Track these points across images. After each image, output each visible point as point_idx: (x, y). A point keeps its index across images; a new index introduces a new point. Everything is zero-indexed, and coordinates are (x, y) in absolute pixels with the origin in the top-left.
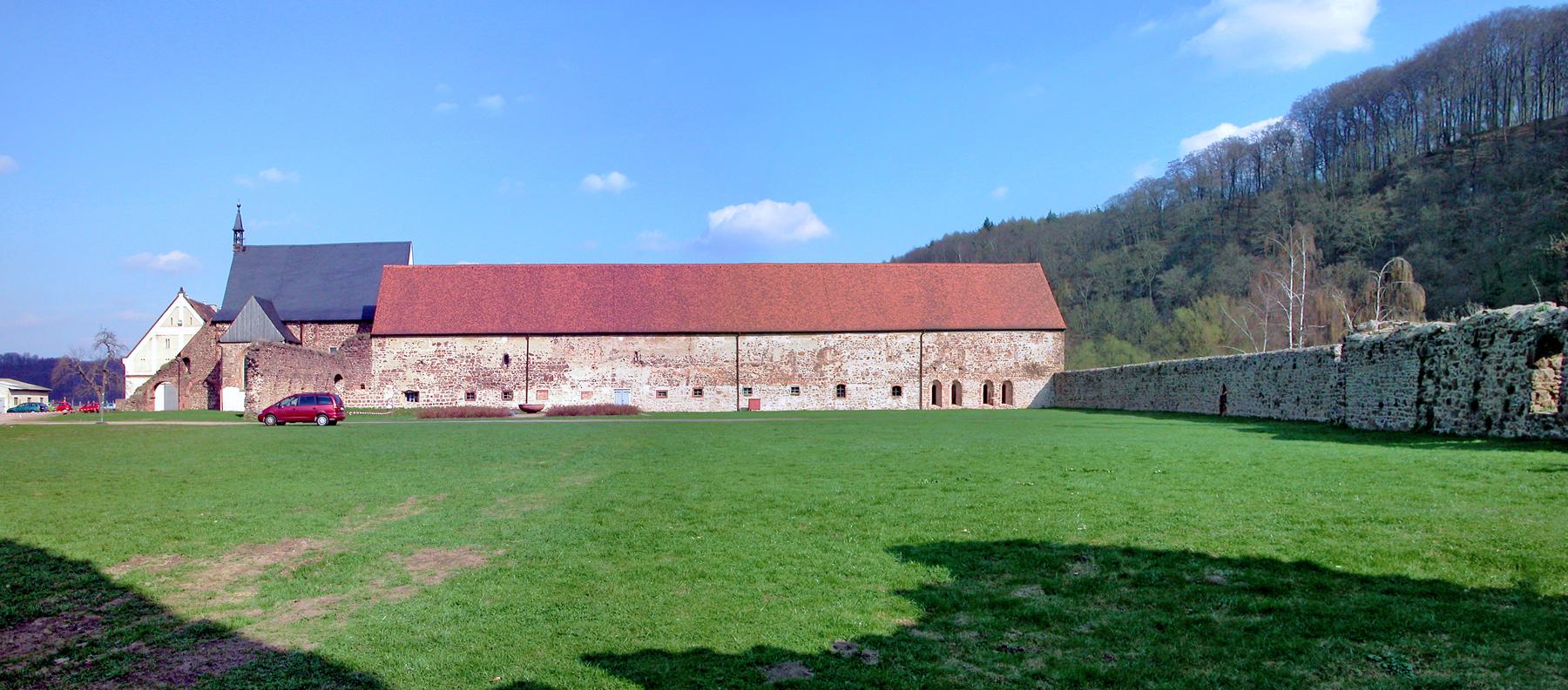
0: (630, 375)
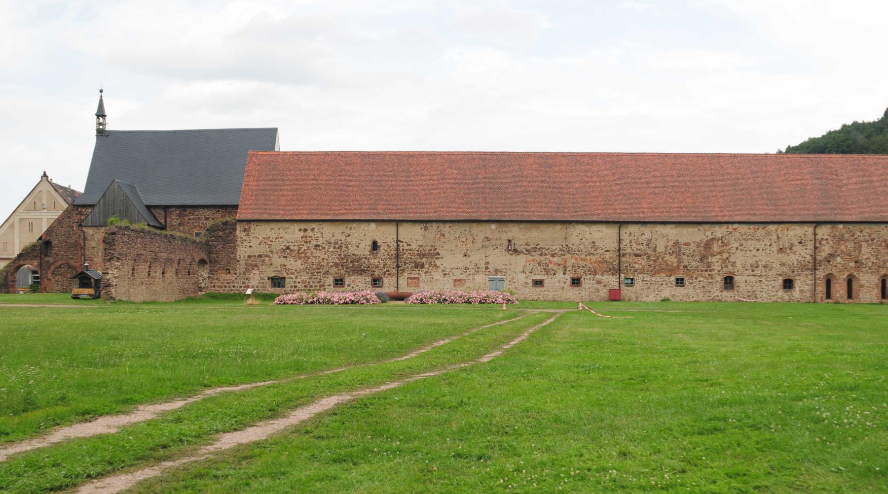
0: (504, 263)
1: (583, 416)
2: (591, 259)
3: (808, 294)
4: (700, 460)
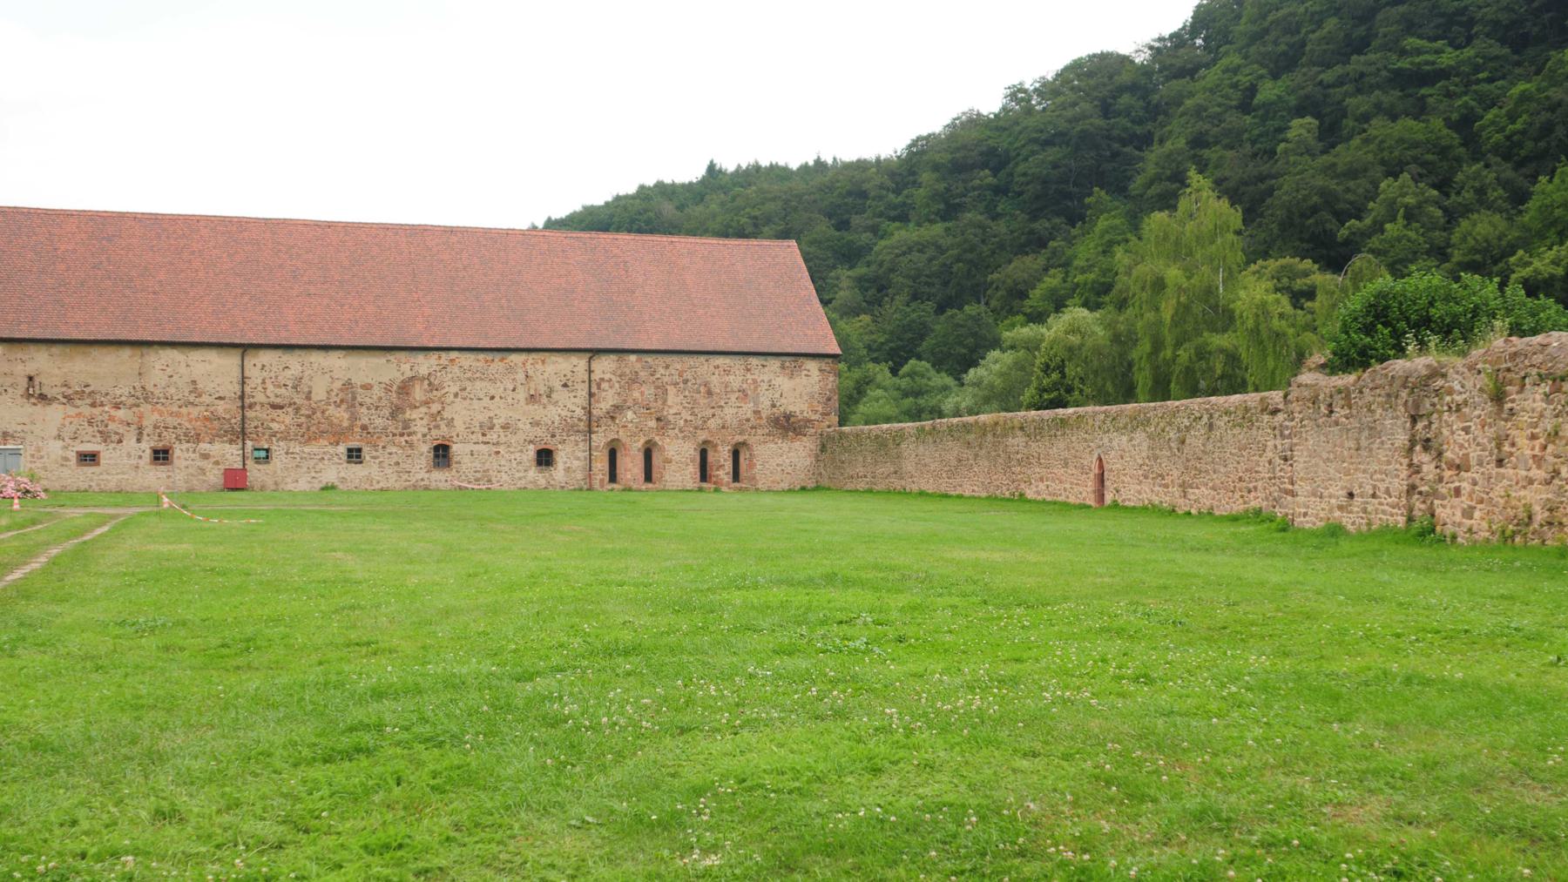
0: (20, 420)
1: (94, 734)
2: (189, 414)
3: (580, 476)
4: (317, 818)
